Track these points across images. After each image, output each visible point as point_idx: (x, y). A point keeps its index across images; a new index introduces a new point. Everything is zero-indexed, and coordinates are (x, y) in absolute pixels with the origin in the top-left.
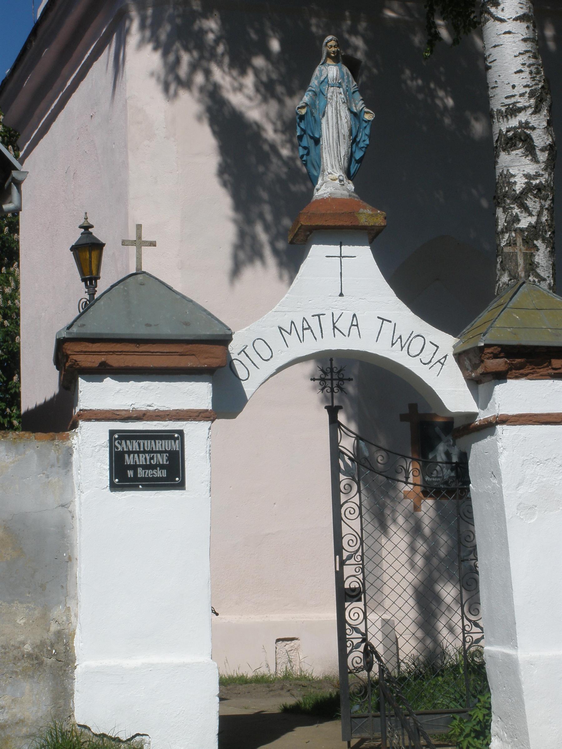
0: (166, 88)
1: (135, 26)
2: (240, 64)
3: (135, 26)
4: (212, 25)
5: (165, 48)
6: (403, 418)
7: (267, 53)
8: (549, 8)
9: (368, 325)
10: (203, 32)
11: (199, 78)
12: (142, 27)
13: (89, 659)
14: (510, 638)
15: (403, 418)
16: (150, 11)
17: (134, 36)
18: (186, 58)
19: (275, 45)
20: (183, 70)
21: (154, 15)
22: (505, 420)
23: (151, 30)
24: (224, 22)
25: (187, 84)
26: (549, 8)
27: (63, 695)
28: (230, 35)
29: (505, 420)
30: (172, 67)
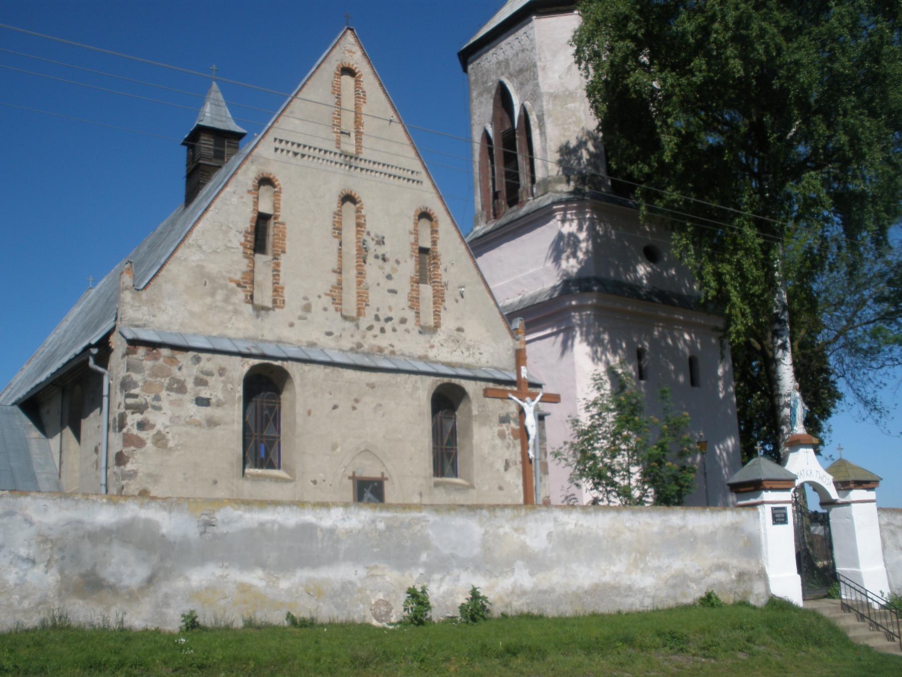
0: (593, 360)
1: (578, 334)
2: (615, 353)
3: (578, 334)
4: (606, 337)
5: (591, 344)
6: (350, 478)
7: (621, 348)
8: (574, 303)
9: (814, 473)
10: (603, 340)
11: (604, 358)
12: (581, 335)
13: (771, 575)
14: (856, 564)
15: (350, 478)
16: (584, 329)
17: (578, 338)
18: (599, 349)
19: (624, 345)
20: (599, 354)
21: (586, 331)
22: (854, 502)
23: (586, 336)
24: (610, 335)
25: (600, 360)
26: (574, 303)
27: (767, 586)
28: (611, 341)
29: (854, 502)
30: (596, 352)
